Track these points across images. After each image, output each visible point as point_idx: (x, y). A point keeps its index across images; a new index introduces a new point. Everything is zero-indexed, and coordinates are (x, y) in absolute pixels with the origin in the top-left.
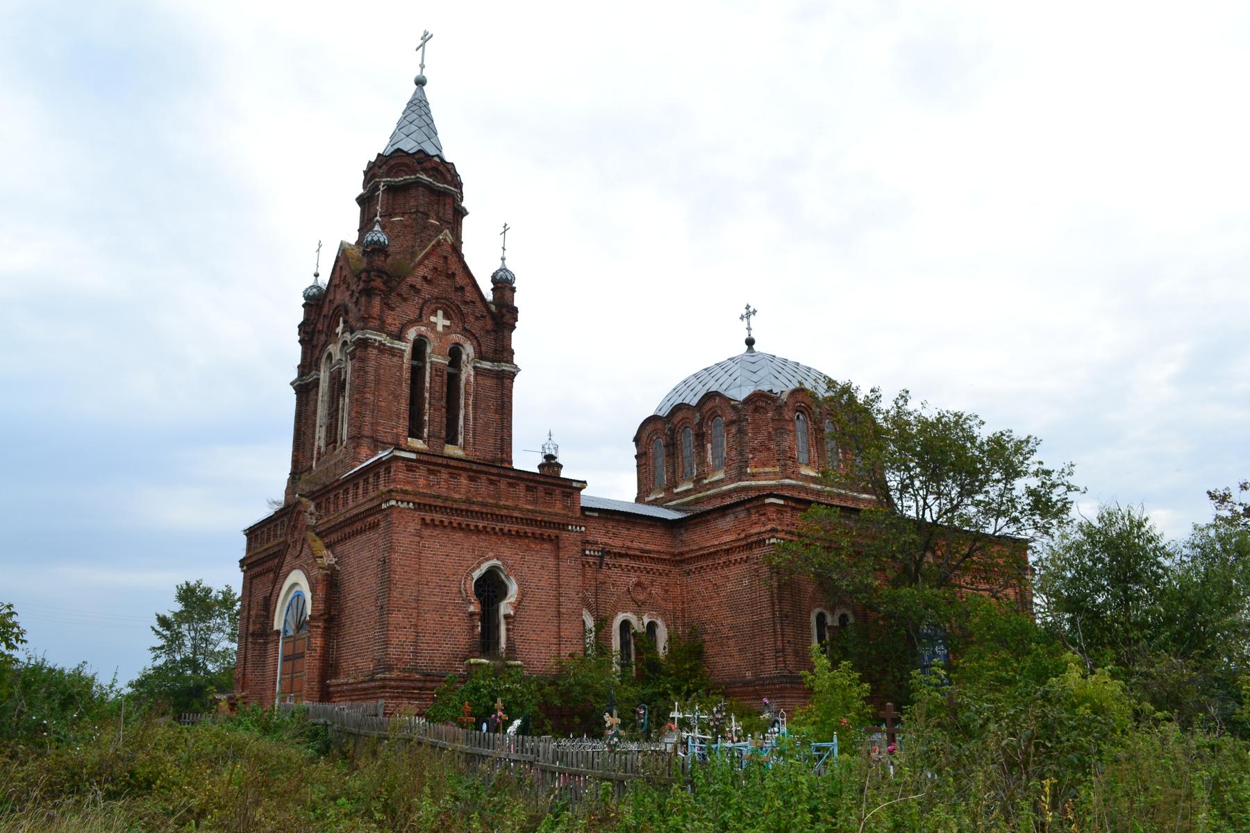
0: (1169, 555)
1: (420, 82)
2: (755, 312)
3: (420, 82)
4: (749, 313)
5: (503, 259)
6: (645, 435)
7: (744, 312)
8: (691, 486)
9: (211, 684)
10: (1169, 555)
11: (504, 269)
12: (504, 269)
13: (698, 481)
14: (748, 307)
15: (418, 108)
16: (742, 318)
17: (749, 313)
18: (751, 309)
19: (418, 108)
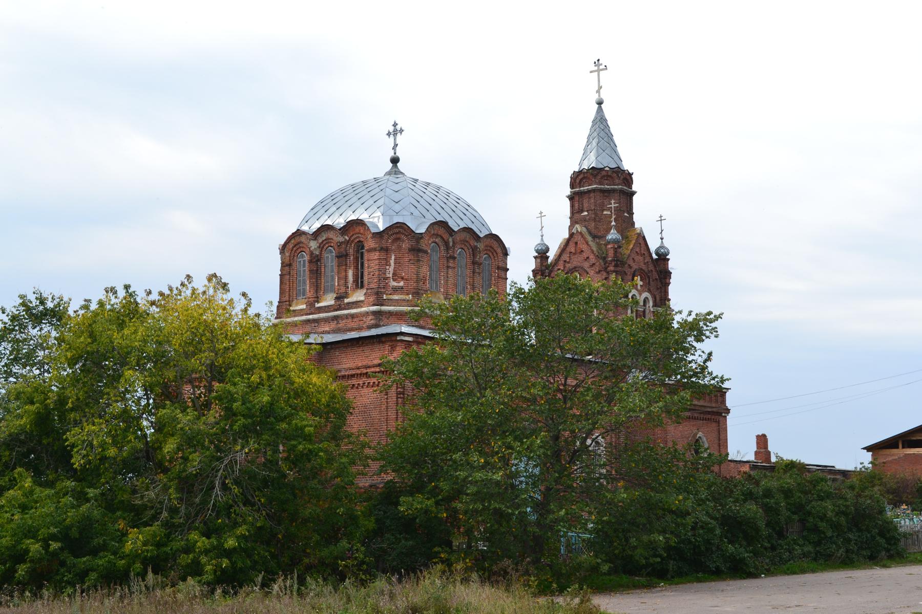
0: (805, 555)
1: (600, 103)
2: (401, 131)
3: (600, 103)
4: (396, 131)
5: (662, 239)
6: (291, 245)
7: (391, 129)
8: (304, 307)
9: (322, 451)
10: (805, 555)
11: (662, 247)
12: (662, 247)
13: (311, 305)
14: (395, 125)
15: (601, 124)
16: (389, 134)
17: (396, 131)
18: (398, 127)
19: (601, 124)
